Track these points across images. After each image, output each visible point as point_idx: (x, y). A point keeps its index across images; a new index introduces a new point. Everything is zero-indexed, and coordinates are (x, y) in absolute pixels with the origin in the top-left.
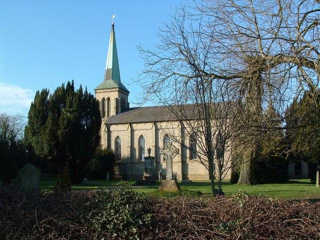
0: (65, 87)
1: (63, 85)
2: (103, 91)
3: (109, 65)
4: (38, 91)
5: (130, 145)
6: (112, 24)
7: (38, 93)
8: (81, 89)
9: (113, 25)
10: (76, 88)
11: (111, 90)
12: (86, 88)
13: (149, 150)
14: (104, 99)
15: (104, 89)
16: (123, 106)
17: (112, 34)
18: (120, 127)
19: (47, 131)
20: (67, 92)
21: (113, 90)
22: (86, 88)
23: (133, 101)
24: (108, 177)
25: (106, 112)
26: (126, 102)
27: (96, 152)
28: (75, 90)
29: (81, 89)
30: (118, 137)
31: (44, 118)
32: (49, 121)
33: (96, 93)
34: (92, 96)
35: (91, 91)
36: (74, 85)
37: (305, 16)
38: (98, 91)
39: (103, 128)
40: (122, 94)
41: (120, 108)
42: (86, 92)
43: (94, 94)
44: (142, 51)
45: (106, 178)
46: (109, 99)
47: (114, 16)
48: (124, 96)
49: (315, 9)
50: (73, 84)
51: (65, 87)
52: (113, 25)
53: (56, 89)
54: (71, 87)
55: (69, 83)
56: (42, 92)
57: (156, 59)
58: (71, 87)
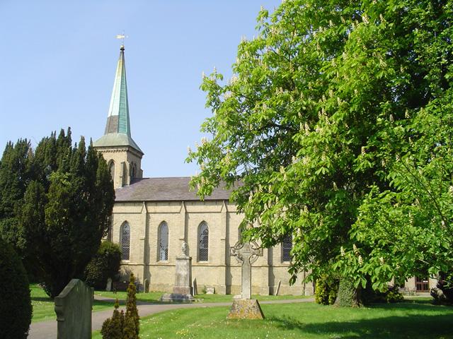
0: (57, 138)
1: (53, 135)
3: (114, 110)
5: (224, 238)
6: (122, 46)
7: (9, 146)
8: (82, 144)
9: (123, 49)
10: (75, 141)
12: (91, 142)
16: (134, 174)
17: (119, 63)
20: (58, 146)
22: (91, 142)
23: (149, 168)
24: (109, 286)
27: (102, 251)
29: (82, 144)
30: (126, 222)
32: (29, 195)
36: (104, 132)
41: (129, 178)
45: (106, 286)
50: (69, 133)
51: (57, 138)
52: (123, 49)
53: (41, 140)
54: (65, 139)
55: (62, 132)
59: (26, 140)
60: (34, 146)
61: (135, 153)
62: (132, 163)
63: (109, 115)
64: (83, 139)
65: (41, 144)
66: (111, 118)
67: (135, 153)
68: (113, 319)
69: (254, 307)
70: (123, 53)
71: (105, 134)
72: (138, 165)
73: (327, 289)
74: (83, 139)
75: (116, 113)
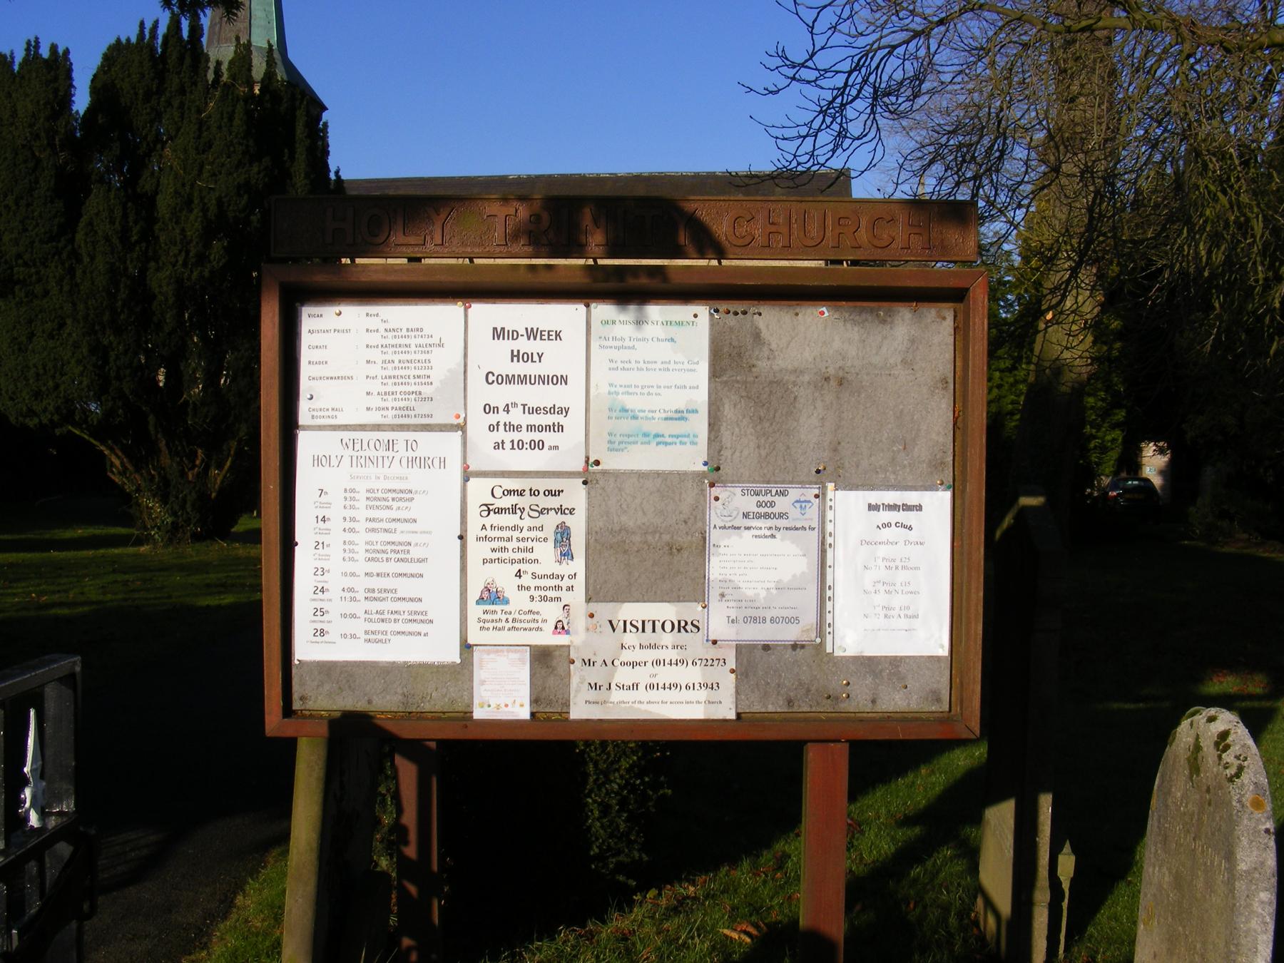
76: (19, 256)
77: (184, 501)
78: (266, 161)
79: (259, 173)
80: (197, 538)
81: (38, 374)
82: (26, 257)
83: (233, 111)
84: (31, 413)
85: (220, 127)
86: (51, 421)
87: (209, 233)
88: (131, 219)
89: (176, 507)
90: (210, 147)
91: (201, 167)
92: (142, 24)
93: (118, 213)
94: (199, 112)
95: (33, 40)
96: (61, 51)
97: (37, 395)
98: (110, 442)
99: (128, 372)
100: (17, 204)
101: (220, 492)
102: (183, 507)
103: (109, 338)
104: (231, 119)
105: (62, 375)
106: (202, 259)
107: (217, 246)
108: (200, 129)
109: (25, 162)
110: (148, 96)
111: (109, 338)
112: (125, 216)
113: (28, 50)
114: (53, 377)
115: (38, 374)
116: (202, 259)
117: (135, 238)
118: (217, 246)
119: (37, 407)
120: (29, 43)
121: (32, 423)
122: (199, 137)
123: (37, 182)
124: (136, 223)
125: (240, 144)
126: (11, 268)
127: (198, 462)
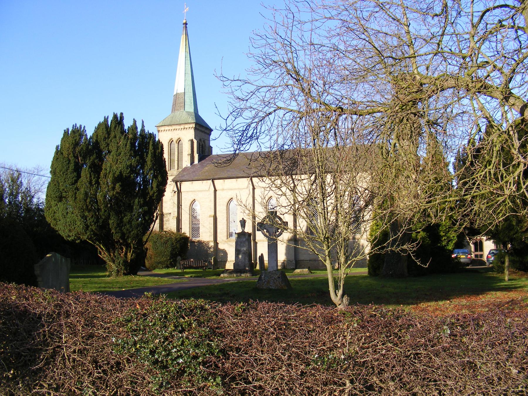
1: (106, 120)
2: (170, 128)
4: (68, 129)
6: (184, 21)
7: (66, 132)
9: (186, 24)
10: (127, 124)
11: (182, 127)
12: (143, 126)
13: (243, 223)
14: (171, 142)
15: (171, 125)
18: (197, 185)
19: (80, 195)
21: (186, 126)
22: (143, 126)
25: (176, 162)
26: (207, 145)
28: (126, 127)
31: (78, 169)
33: (159, 131)
34: (152, 136)
35: (150, 129)
37: (482, 17)
38: (162, 128)
39: (170, 187)
40: (203, 134)
42: (143, 130)
43: (155, 132)
44: (223, 78)
46: (179, 141)
47: (48, 255)
48: (203, 136)
49: (496, 5)
52: (186, 24)
54: (118, 121)
55: (115, 116)
56: (73, 132)
57: (252, 88)
58: (118, 121)
59: (81, 126)
60: (90, 132)
61: (203, 130)
62: (200, 140)
63: (175, 93)
64: (135, 122)
65: (97, 129)
66: (177, 96)
67: (203, 130)
68: (270, 272)
69: (279, 277)
70: (186, 27)
71: (172, 112)
72: (207, 142)
73: (492, 126)
74: (135, 122)
75: (181, 90)
76: (63, 190)
77: (120, 263)
78: (138, 158)
79: (134, 161)
80: (125, 274)
81: (69, 225)
82: (65, 190)
83: (127, 143)
84: (69, 236)
85: (123, 148)
86: (74, 238)
87: (114, 182)
88: (93, 177)
89: (117, 265)
90: (121, 154)
91: (117, 160)
92: (105, 117)
93: (88, 176)
94: (118, 144)
95: (75, 124)
96: (119, 115)
97: (70, 231)
98: (265, 230)
99: (93, 223)
100: (63, 174)
101: (131, 260)
102: (120, 265)
103: (86, 214)
104: (126, 146)
105: (76, 225)
106: (114, 188)
107: (118, 185)
108: (118, 149)
109: (66, 161)
110: (105, 138)
111: (86, 214)
112: (91, 176)
113: (73, 127)
114: (73, 225)
115: (69, 225)
116: (114, 188)
117: (93, 183)
118: (118, 185)
119: (71, 234)
120: (73, 126)
121: (70, 239)
122: (117, 151)
123: (69, 167)
124: (94, 178)
125: (128, 153)
126: (62, 193)
127: (124, 251)
